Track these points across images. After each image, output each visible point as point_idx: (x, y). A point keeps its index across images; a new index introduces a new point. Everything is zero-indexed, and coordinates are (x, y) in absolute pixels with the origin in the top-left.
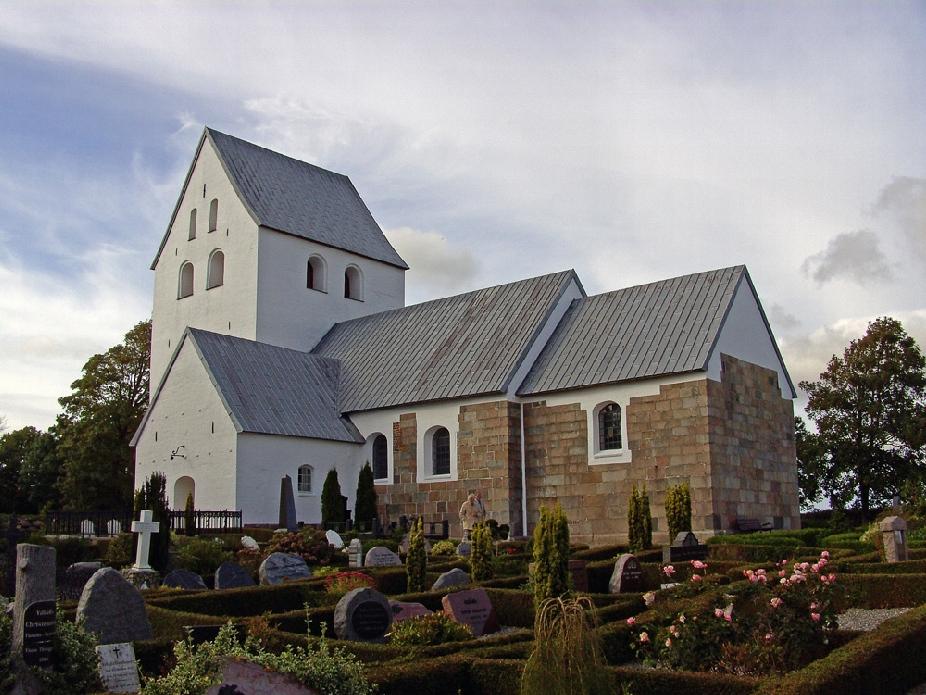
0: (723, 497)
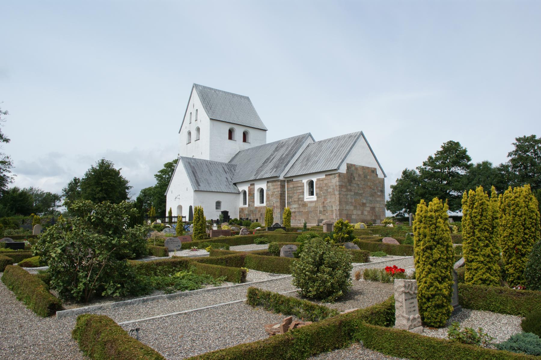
0: (345, 212)
